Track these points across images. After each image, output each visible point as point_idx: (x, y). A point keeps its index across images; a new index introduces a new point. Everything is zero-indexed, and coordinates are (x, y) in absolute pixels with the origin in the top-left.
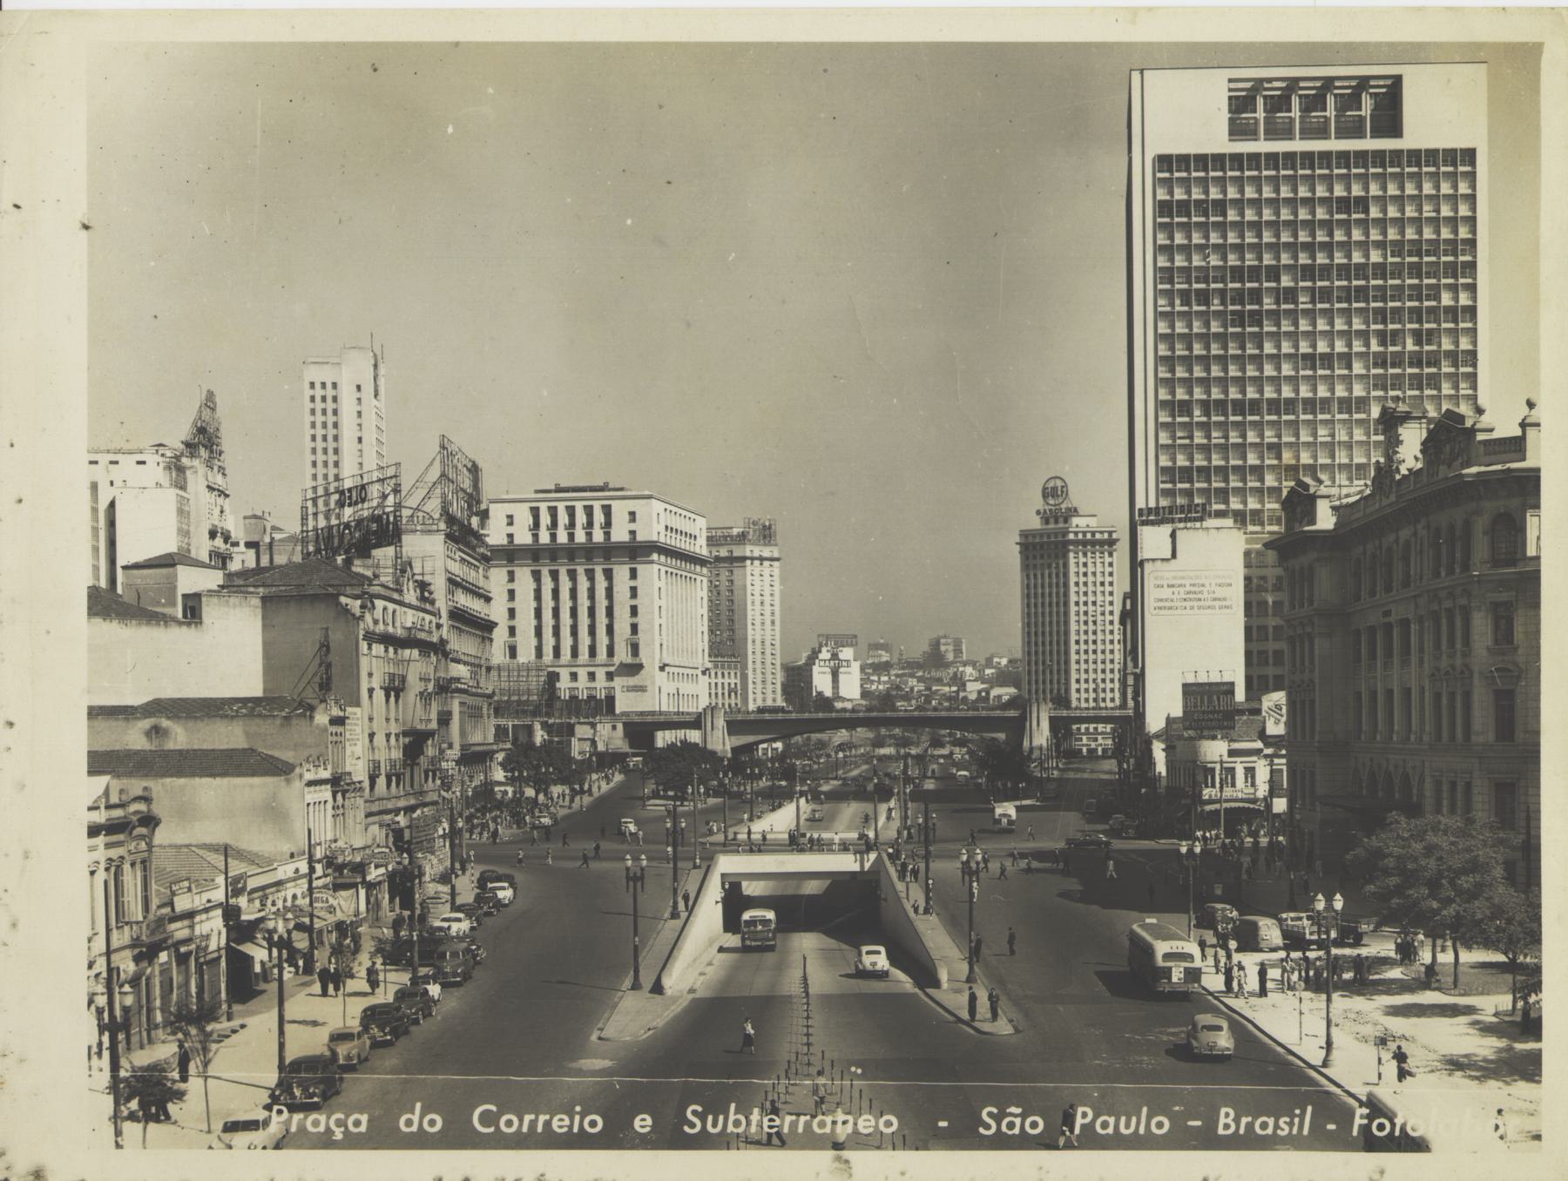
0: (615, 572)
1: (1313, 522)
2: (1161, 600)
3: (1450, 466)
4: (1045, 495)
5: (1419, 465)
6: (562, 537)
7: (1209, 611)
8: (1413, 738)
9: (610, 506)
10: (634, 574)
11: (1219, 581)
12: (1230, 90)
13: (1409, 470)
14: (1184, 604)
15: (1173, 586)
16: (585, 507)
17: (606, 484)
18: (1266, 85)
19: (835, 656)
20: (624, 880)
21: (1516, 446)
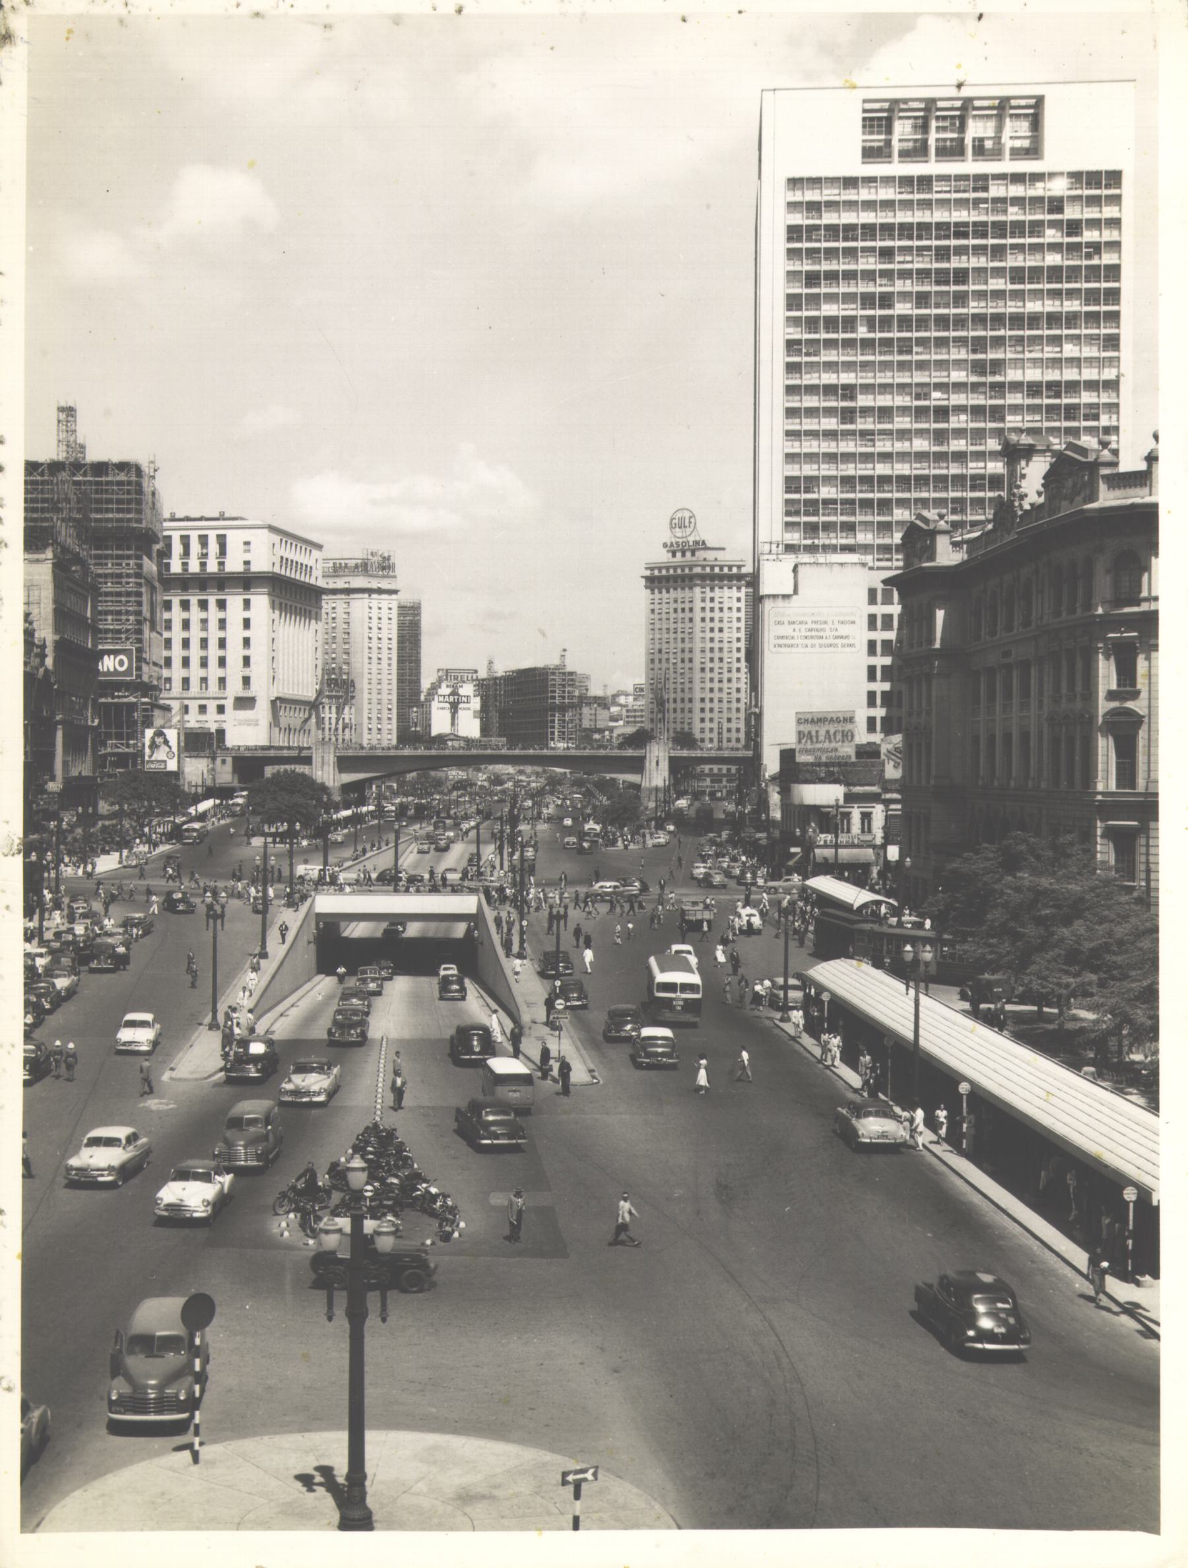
0: (228, 603)
1: (932, 557)
3: (1072, 502)
5: (1042, 500)
7: (832, 649)
8: (1030, 784)
9: (225, 536)
10: (247, 604)
12: (865, 111)
13: (1031, 505)
15: (794, 623)
16: (200, 536)
17: (173, 514)
18: (903, 106)
19: (454, 693)
20: (205, 917)
21: (1143, 478)
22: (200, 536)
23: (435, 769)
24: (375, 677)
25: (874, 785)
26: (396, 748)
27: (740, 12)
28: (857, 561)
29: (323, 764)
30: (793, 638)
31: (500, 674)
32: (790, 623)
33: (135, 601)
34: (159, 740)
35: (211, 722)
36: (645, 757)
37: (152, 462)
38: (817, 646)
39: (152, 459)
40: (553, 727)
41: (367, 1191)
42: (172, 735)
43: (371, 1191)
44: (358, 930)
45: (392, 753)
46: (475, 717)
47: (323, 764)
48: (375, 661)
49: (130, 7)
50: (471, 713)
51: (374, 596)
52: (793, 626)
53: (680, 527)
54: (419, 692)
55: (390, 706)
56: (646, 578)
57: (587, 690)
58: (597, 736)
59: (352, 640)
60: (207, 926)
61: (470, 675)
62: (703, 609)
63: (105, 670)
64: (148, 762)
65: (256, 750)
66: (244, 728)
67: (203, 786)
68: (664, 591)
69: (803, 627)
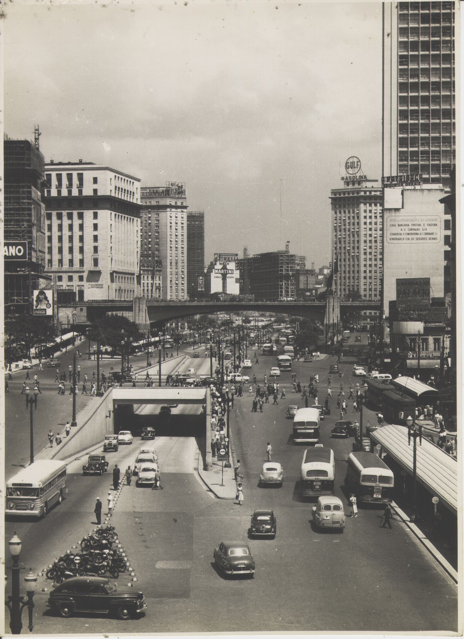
0: (84, 215)
2: (394, 234)
4: (347, 167)
6: (65, 193)
9: (82, 174)
10: (96, 216)
11: (429, 223)
14: (408, 236)
15: (401, 225)
17: (52, 162)
19: (224, 268)
22: (78, 174)
23: (212, 313)
24: (174, 259)
25: (441, 322)
26: (189, 301)
27: (299, 5)
28: (438, 188)
29: (139, 311)
30: (401, 234)
31: (251, 256)
32: (399, 225)
33: (28, 214)
34: (42, 297)
35: (75, 284)
36: (326, 305)
37: (37, 130)
38: (415, 239)
39: (37, 128)
40: (282, 288)
41: (76, 560)
42: (49, 294)
43: (79, 560)
44: (146, 410)
45: (187, 304)
46: (236, 282)
47: (139, 311)
48: (174, 249)
49: (52, 3)
50: (234, 280)
51: (173, 210)
52: (402, 227)
53: (351, 168)
54: (203, 268)
55: (183, 276)
56: (441, 201)
57: (305, 266)
58: (308, 294)
59: (160, 237)
60: (27, 407)
61: (233, 257)
62: (365, 217)
63: (10, 255)
64: (35, 310)
65: (92, 302)
66: (95, 289)
67: (68, 324)
68: (373, 205)
69: (407, 228)
